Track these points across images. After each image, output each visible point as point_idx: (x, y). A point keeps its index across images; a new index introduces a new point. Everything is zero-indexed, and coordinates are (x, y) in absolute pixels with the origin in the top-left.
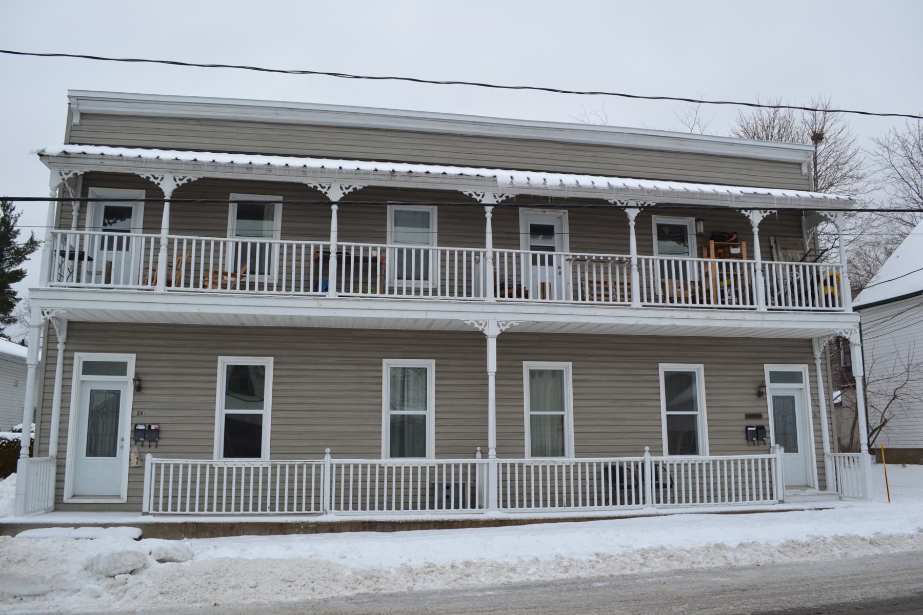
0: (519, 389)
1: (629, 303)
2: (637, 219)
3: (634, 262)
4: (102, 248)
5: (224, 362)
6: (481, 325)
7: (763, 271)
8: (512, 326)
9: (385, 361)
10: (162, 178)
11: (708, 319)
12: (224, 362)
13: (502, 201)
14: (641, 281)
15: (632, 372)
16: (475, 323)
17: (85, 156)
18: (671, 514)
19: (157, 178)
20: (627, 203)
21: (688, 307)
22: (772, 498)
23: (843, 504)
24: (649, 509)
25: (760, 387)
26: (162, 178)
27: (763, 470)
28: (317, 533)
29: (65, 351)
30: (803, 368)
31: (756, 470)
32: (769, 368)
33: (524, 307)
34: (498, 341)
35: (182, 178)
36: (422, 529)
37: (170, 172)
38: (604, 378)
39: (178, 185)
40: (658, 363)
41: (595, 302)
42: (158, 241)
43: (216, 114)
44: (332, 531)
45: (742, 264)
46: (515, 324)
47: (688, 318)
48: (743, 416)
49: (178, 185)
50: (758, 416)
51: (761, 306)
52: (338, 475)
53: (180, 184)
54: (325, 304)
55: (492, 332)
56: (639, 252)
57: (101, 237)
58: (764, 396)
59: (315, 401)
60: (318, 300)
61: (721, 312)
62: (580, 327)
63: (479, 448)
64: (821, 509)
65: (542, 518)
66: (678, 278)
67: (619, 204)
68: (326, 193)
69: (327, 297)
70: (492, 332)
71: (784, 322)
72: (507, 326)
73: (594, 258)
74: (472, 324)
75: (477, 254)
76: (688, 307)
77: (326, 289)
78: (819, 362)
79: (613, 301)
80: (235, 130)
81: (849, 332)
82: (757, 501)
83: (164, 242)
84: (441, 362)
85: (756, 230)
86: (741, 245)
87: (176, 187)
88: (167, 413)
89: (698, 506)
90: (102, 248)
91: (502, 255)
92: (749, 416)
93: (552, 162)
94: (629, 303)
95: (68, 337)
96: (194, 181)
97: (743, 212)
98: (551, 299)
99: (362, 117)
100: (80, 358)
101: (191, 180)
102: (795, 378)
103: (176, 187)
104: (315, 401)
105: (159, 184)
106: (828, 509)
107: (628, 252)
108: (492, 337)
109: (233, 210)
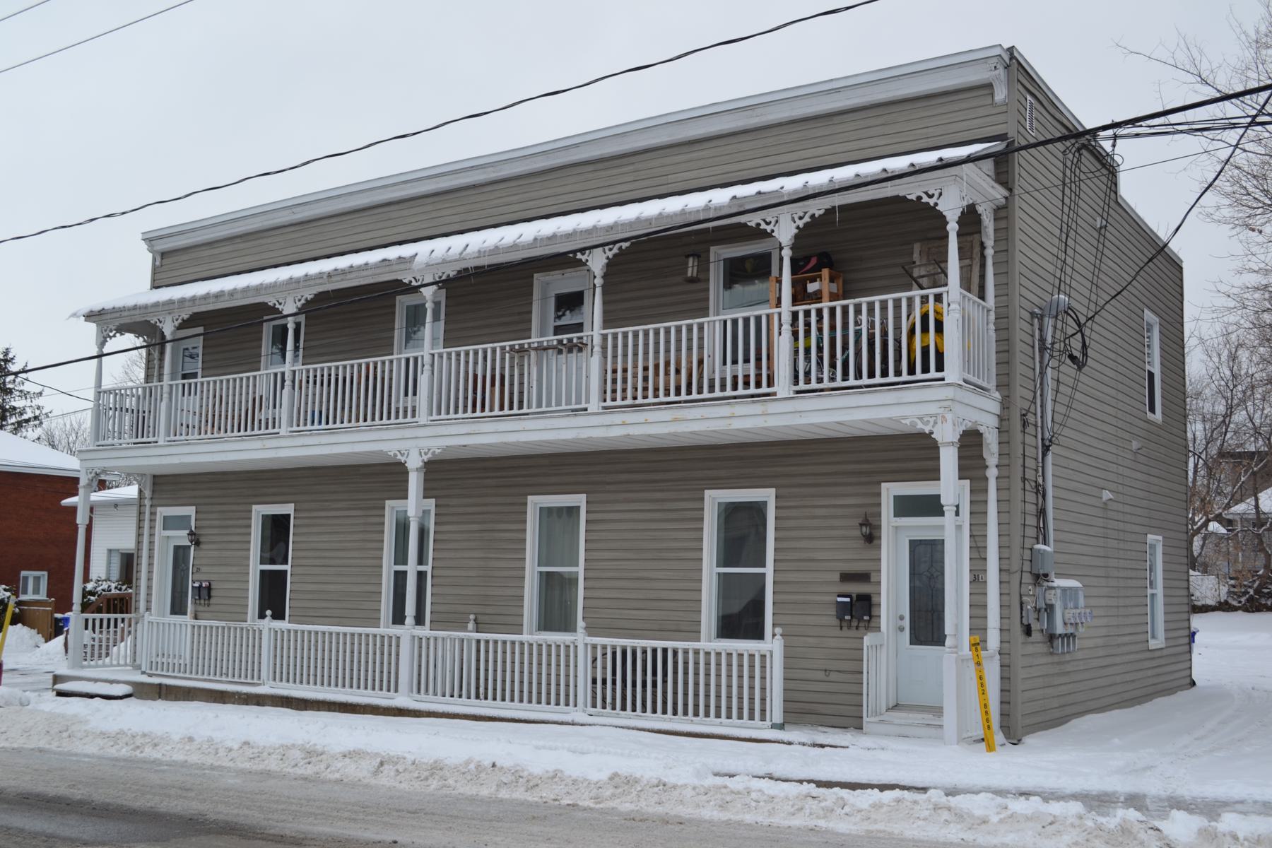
1: (939, 375)
4: (183, 395)
5: (714, 498)
8: (434, 453)
9: (708, 494)
10: (941, 194)
11: (676, 420)
12: (259, 511)
17: (387, 263)
18: (590, 725)
19: (933, 195)
20: (423, 280)
21: (680, 402)
22: (763, 718)
23: (864, 741)
24: (578, 715)
26: (941, 194)
28: (247, 704)
29: (151, 506)
32: (891, 491)
33: (444, 427)
35: (802, 214)
36: (329, 710)
37: (170, 313)
38: (628, 516)
39: (798, 227)
40: (703, 490)
43: (237, 230)
44: (258, 704)
47: (646, 423)
48: (837, 577)
49: (798, 227)
50: (864, 577)
51: (783, 386)
53: (801, 226)
54: (773, 407)
55: (414, 463)
57: (722, 322)
58: (875, 542)
59: (327, 554)
60: (262, 439)
61: (694, 406)
64: (822, 746)
65: (441, 711)
66: (475, 376)
67: (414, 283)
68: (936, 204)
69: (589, 411)
71: (803, 414)
72: (430, 455)
73: (517, 347)
74: (395, 455)
76: (680, 402)
80: (269, 240)
82: (622, 712)
84: (442, 501)
86: (820, 277)
87: (796, 231)
88: (216, 569)
89: (618, 716)
90: (183, 395)
92: (847, 577)
93: (579, 195)
94: (939, 375)
95: (153, 491)
96: (820, 216)
97: (579, 256)
99: (368, 193)
100: (163, 511)
101: (814, 215)
103: (796, 231)
104: (327, 554)
106: (836, 747)
108: (413, 471)
109: (716, 275)
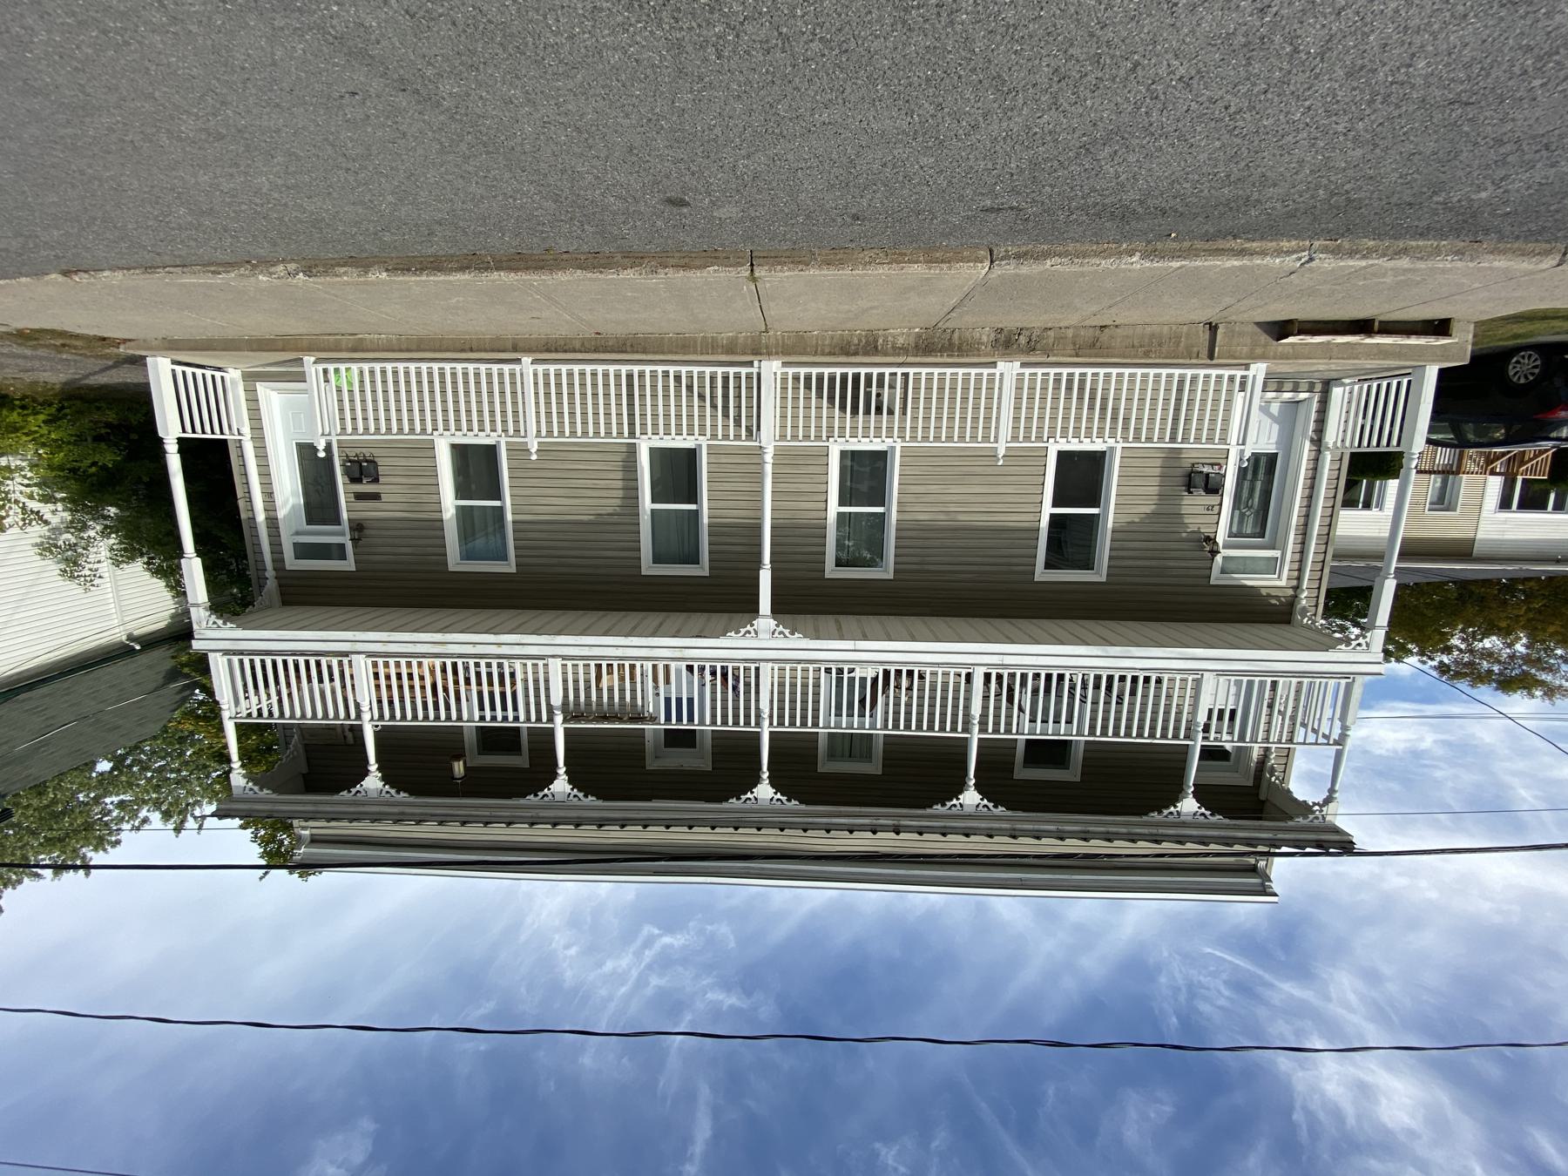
0: (713, 538)
2: (366, 773)
3: (559, 718)
6: (780, 633)
7: (758, 716)
13: (1167, 807)
14: (757, 701)
15: (555, 561)
16: (788, 635)
25: (359, 539)
27: (457, 411)
30: (292, 563)
31: (445, 411)
32: (349, 565)
34: (757, 611)
41: (719, 666)
42: (983, 730)
45: (714, 723)
46: (733, 634)
50: (360, 497)
52: (987, 428)
55: (765, 621)
56: (551, 733)
62: (520, 625)
63: (1000, 463)
70: (765, 621)
75: (781, 724)
77: (987, 676)
78: (270, 572)
79: (537, 665)
81: (776, 635)
83: (766, 723)
85: (562, 770)
91: (747, 723)
98: (444, 664)
102: (303, 551)
105: (982, 799)
107: (567, 732)
